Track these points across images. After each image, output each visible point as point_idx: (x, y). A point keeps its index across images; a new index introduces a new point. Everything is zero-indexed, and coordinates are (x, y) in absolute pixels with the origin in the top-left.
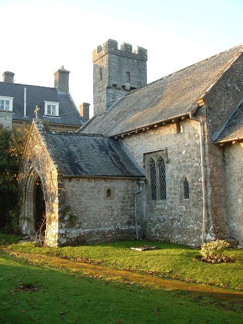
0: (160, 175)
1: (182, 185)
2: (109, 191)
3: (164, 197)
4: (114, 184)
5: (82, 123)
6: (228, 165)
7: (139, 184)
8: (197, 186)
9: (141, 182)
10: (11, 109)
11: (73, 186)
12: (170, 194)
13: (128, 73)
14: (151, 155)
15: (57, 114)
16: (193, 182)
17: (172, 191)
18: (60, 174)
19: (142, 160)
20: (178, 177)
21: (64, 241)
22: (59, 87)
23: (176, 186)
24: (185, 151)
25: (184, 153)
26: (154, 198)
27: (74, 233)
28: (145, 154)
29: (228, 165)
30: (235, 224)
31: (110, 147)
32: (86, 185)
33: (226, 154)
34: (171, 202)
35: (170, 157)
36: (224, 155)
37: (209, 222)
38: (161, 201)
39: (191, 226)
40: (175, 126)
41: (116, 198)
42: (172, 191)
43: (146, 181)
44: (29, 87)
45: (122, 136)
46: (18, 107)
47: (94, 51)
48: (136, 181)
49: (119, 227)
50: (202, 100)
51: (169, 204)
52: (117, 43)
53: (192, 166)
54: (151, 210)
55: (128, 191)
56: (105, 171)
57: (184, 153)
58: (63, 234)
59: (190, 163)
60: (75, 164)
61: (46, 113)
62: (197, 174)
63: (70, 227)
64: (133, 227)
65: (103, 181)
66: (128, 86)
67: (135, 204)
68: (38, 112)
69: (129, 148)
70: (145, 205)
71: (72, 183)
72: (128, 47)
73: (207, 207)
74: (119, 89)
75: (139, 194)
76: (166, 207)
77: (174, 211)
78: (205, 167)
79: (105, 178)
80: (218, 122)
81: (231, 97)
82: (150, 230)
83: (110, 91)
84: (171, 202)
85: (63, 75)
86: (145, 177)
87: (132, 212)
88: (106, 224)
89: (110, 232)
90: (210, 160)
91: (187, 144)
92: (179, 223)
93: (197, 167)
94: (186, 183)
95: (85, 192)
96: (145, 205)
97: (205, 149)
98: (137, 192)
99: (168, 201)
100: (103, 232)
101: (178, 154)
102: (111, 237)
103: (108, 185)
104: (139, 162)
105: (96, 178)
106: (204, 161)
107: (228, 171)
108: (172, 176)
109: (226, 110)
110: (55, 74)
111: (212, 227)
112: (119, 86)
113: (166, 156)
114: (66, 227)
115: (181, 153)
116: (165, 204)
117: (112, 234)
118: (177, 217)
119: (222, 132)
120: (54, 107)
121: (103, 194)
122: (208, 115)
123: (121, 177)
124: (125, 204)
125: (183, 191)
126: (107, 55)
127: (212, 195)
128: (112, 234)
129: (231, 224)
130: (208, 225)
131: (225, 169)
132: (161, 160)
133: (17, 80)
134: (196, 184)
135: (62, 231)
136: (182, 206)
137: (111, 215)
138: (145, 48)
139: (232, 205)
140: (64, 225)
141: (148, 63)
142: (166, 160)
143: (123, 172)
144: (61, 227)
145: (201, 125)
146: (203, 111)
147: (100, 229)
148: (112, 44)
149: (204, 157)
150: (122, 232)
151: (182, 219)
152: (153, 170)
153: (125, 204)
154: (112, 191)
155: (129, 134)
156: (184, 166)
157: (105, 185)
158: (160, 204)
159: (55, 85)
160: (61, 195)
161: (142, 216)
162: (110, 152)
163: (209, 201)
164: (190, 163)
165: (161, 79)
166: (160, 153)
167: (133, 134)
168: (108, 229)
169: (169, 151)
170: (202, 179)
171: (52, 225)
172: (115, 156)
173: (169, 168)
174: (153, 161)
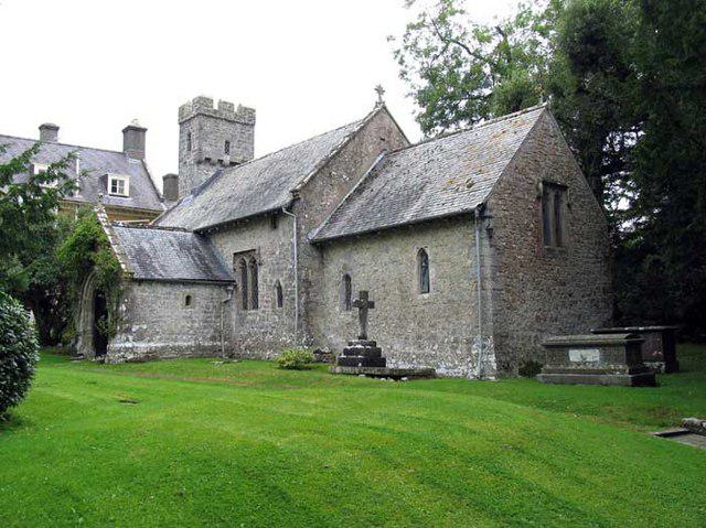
3: (256, 307)
20: (271, 281)
38: (252, 311)
85: (134, 134)
108: (265, 281)
115: (274, 253)
140: (131, 338)
150: (205, 349)
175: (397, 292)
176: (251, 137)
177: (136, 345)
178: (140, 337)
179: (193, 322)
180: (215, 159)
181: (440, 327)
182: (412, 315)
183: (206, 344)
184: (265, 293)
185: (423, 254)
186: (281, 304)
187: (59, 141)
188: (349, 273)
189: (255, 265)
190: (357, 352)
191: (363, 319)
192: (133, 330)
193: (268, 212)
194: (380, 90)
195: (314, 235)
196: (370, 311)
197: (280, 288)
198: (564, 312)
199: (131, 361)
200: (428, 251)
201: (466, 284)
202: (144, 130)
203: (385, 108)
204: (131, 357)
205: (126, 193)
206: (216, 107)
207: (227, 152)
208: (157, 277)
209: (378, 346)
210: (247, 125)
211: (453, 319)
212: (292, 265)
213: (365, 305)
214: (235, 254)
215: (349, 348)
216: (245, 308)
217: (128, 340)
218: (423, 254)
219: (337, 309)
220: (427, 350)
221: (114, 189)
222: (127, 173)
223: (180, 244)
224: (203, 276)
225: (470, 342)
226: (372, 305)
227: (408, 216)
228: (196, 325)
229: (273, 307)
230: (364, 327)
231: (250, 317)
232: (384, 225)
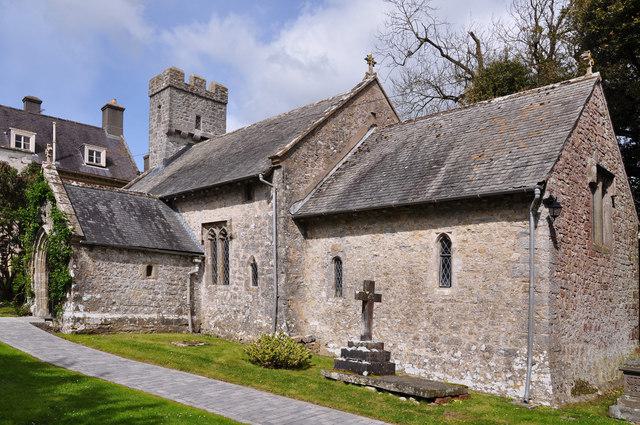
3: (226, 282)
13: (198, 118)
16: (263, 264)
17: (237, 275)
20: (245, 257)
25: (252, 226)
26: (215, 282)
31: (158, 211)
38: (223, 287)
39: (259, 321)
42: (237, 275)
53: (262, 245)
85: (114, 112)
108: (237, 256)
115: (247, 226)
127: (286, 284)
133: (47, 110)
140: (81, 307)
143: (171, 245)
147: (136, 316)
150: (168, 322)
151: (248, 311)
162: (157, 218)
167: (430, 42)
168: (147, 316)
171: (503, 44)
172: (163, 224)
175: (405, 283)
176: (224, 114)
177: (88, 315)
178: (93, 306)
179: (157, 294)
180: (185, 131)
181: (467, 329)
182: (425, 312)
183: (171, 317)
184: (238, 270)
185: (445, 241)
186: (255, 284)
187: (43, 113)
188: (340, 255)
189: (226, 238)
190: (363, 356)
191: (368, 314)
192: (84, 299)
193: (242, 181)
194: (370, 61)
195: (297, 209)
196: (376, 304)
197: (254, 266)
198: (606, 320)
199: (82, 333)
200: (452, 238)
201: (507, 283)
202: (122, 110)
203: (376, 81)
204: (81, 327)
205: (103, 163)
206: (187, 81)
207: (197, 127)
208: (111, 243)
209: (386, 348)
210: (220, 103)
211: (485, 323)
212: (269, 241)
213: (369, 298)
214: (204, 225)
215: (349, 349)
216: (215, 282)
217: (77, 309)
218: (445, 241)
219: (324, 294)
220: (445, 356)
221: (91, 159)
222: (104, 146)
223: (141, 210)
224: (166, 246)
225: (510, 354)
226: (378, 298)
227: (431, 191)
228: (159, 296)
229: (247, 284)
230: (369, 325)
231: (219, 293)
232: (230, 265)
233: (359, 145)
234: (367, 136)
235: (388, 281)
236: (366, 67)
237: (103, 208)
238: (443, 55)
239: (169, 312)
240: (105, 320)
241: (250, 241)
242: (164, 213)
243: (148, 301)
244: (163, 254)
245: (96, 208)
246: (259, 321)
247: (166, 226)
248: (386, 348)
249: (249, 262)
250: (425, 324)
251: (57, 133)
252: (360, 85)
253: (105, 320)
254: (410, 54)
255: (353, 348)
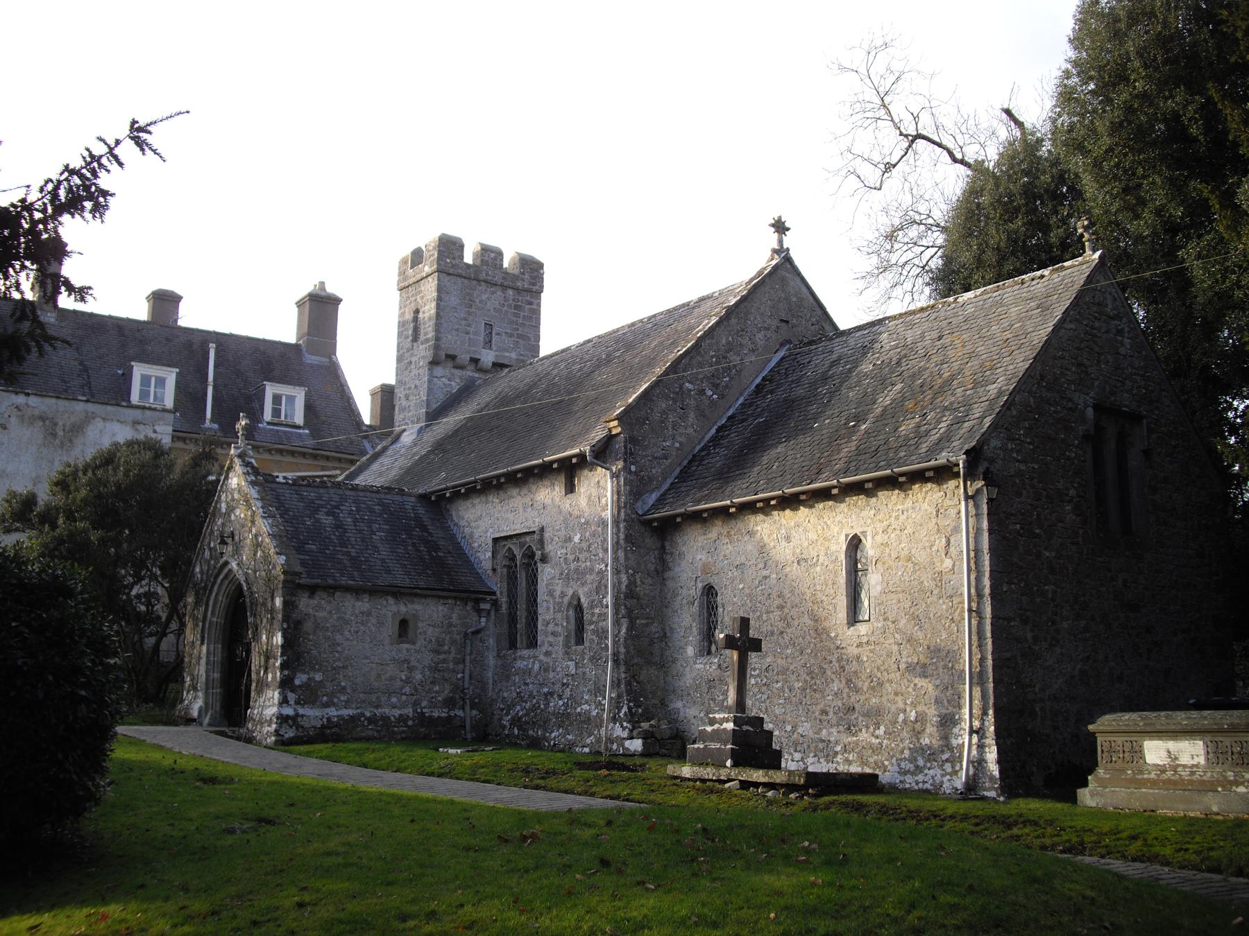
0: (528, 590)
1: (571, 613)
2: (404, 624)
3: (533, 643)
4: (417, 607)
5: (367, 445)
6: (670, 569)
7: (479, 612)
8: (600, 615)
9: (483, 606)
10: (169, 402)
11: (319, 608)
12: (546, 634)
13: (489, 326)
14: (509, 544)
15: (299, 419)
18: (289, 578)
19: (489, 554)
20: (563, 595)
21: (290, 734)
22: (309, 343)
23: (559, 616)
24: (579, 536)
25: (577, 539)
27: (313, 715)
28: (496, 540)
29: (670, 569)
30: (679, 704)
32: (355, 606)
33: (667, 545)
34: (547, 654)
35: (549, 548)
36: (663, 547)
37: (619, 696)
38: (526, 652)
40: (562, 478)
41: (421, 642)
42: (551, 628)
43: (495, 604)
44: (222, 340)
45: (448, 495)
46: (189, 397)
47: (404, 262)
48: (470, 604)
49: (424, 710)
50: (615, 423)
51: (542, 657)
52: (462, 247)
53: (591, 570)
54: (505, 672)
55: (450, 625)
56: (400, 578)
57: (577, 539)
58: (288, 717)
59: (588, 564)
60: (31, 508)
61: (268, 415)
62: (600, 588)
63: (305, 703)
64: (460, 713)
65: (391, 600)
66: (488, 357)
67: (468, 658)
68: (245, 428)
69: (462, 523)
70: (491, 660)
71: (314, 602)
72: (490, 255)
73: (616, 662)
74: (462, 368)
75: (479, 636)
76: (537, 666)
77: (551, 675)
78: (617, 572)
79: (397, 593)
80: (654, 471)
81: (692, 415)
82: (500, 719)
83: (439, 371)
84: (547, 654)
86: (494, 593)
87: (459, 676)
88: (394, 700)
89: (402, 719)
90: (626, 558)
91: (583, 521)
92: (561, 703)
93: (601, 572)
94: (579, 608)
95: (347, 622)
96: (491, 660)
97: (619, 530)
98: (473, 629)
99: (540, 652)
100: (385, 719)
101: (566, 541)
102: (404, 732)
103: (403, 609)
104: (484, 557)
105: (375, 592)
106: (616, 559)
107: (670, 584)
108: (551, 593)
109: (677, 445)
110: (300, 304)
111: (625, 709)
112: (464, 358)
113: (539, 547)
114: (297, 703)
115: (570, 539)
116: (535, 657)
117: (407, 726)
118: (557, 687)
119: (662, 495)
120: (291, 399)
121: (391, 628)
122: (629, 457)
123: (434, 593)
124: (442, 657)
125: (572, 627)
126: (436, 274)
128: (407, 726)
129: (672, 706)
130: (616, 703)
131: (664, 579)
132: (530, 555)
133: (189, 317)
134: (597, 611)
135: (288, 711)
136: (570, 663)
137: (407, 681)
138: (539, 256)
139: (674, 661)
140: (292, 697)
141: (546, 298)
142: (539, 553)
144: (284, 701)
145: (612, 478)
146: (619, 445)
147: (378, 712)
148: (449, 247)
149: (615, 552)
150: (432, 722)
151: (568, 692)
152: (512, 579)
153: (442, 657)
154: (411, 625)
155: (463, 491)
156: (577, 570)
157: (392, 609)
158: (525, 659)
159: (298, 339)
160: (289, 627)
161: (484, 689)
162: (417, 532)
163: (622, 650)
164: (588, 564)
165: (563, 351)
166: (528, 539)
168: (397, 712)
169: (547, 535)
170: (609, 600)
173: (546, 573)
174: (512, 558)
188: (714, 581)
192: (297, 682)
207: (488, 343)
210: (528, 291)
226: (756, 645)
233: (758, 380)
234: (773, 364)
235: (784, 619)
236: (772, 239)
237: (327, 521)
238: (955, 160)
239: (432, 705)
240: (329, 719)
241: (573, 566)
242: (427, 522)
243: (399, 684)
244: (426, 596)
245: (317, 521)
246: (586, 707)
247: (433, 546)
248: (72, 464)
249: (570, 604)
250: (835, 687)
251: (216, 366)
252: (760, 273)
253: (329, 719)
254: (889, 167)
255: (716, 726)
